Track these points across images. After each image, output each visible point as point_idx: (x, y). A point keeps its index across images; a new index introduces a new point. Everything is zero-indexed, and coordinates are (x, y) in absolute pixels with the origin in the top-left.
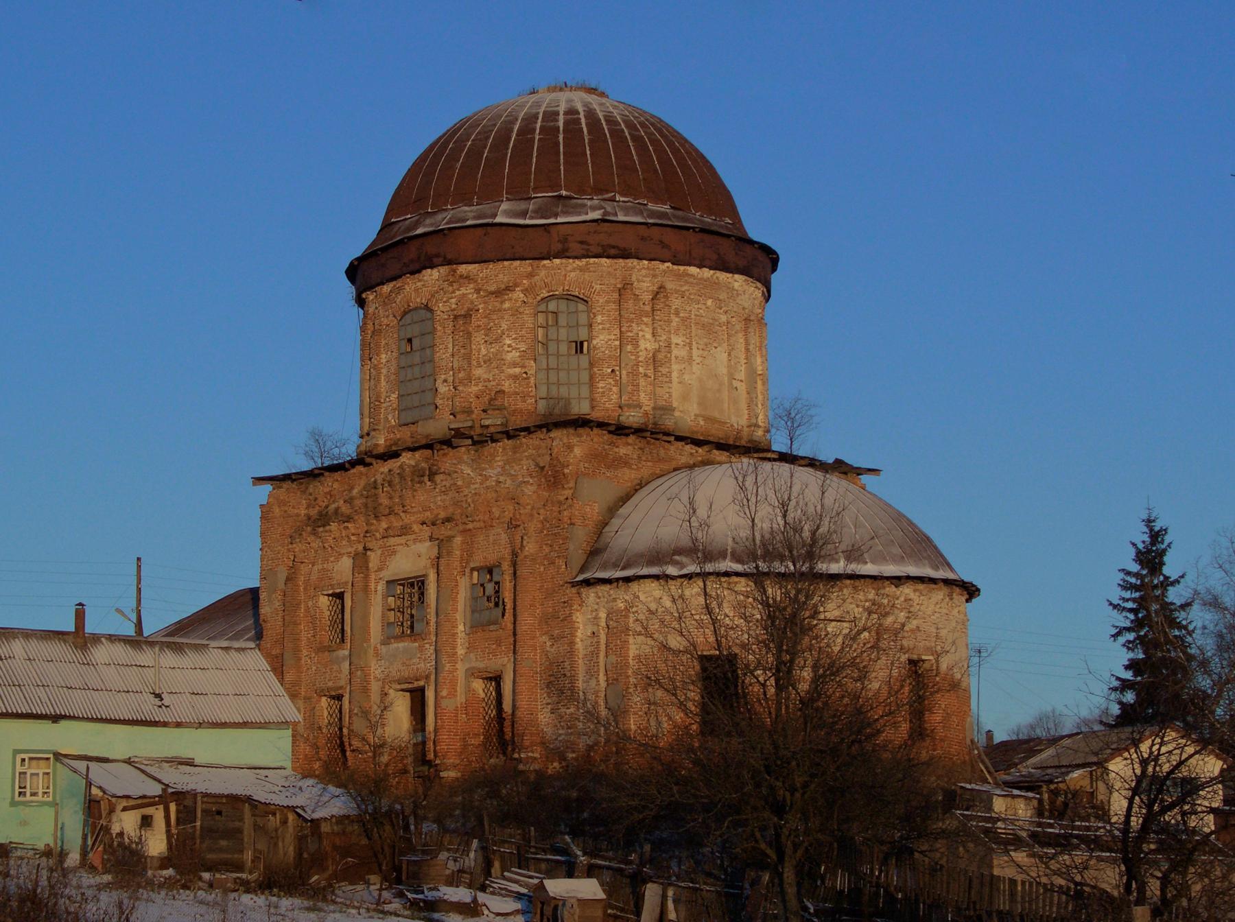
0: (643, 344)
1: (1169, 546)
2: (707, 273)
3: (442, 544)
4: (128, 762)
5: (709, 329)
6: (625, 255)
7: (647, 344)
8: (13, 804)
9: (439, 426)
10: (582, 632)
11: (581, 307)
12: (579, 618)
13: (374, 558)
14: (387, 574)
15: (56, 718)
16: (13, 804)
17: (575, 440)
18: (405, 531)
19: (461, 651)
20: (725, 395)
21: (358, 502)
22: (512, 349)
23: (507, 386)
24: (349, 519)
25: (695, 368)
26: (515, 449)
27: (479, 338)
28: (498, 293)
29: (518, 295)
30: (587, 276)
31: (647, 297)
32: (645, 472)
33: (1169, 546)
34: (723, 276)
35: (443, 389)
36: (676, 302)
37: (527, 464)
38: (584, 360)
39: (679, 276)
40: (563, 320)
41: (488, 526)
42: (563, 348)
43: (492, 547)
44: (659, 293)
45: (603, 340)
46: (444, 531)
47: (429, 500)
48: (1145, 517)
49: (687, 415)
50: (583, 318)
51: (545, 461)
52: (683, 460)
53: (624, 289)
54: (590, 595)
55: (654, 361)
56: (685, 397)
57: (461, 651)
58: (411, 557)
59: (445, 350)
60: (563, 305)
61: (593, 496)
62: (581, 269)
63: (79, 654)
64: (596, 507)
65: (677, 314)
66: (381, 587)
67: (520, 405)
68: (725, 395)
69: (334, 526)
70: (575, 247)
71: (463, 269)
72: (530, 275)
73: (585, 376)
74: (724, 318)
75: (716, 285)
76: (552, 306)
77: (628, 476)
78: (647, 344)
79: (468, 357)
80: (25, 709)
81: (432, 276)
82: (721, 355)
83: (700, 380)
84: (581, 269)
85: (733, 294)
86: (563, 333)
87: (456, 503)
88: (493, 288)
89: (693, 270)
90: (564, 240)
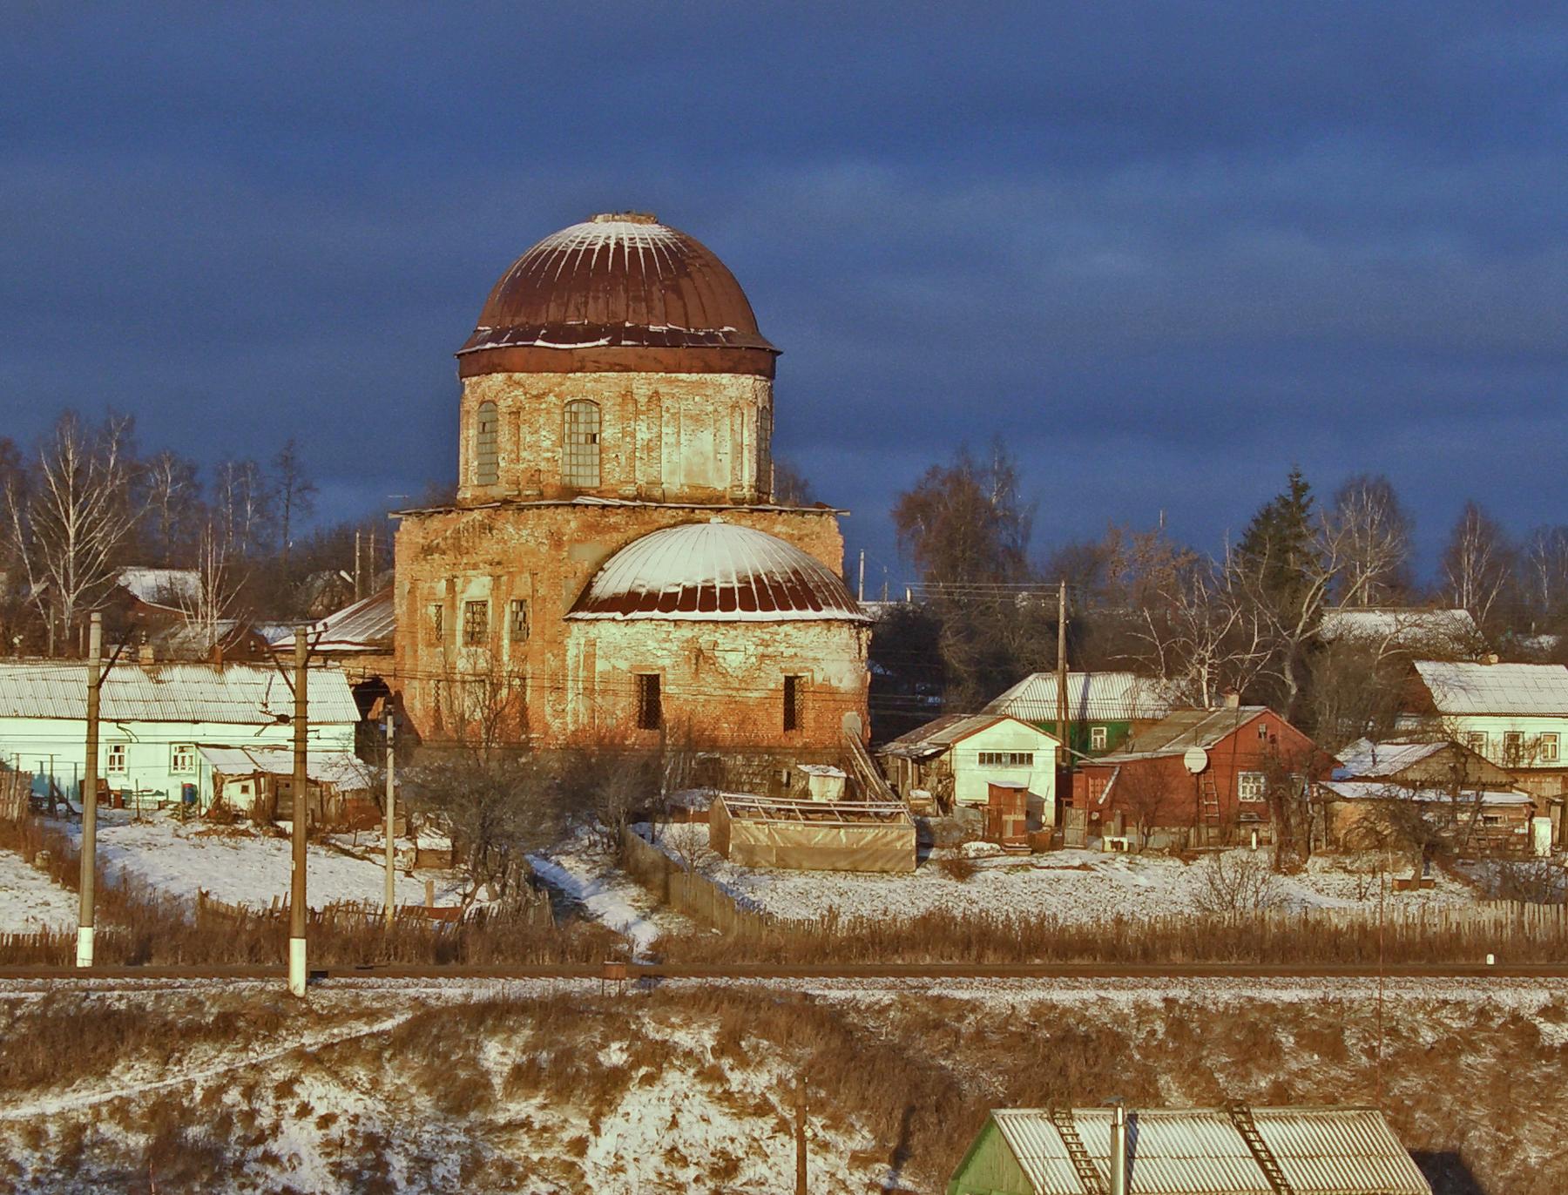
0: (639, 436)
1: (1311, 500)
2: (694, 377)
3: (497, 579)
4: (242, 748)
5: (696, 419)
6: (627, 369)
7: (643, 434)
8: (170, 775)
9: (502, 490)
10: (572, 652)
11: (595, 409)
12: (570, 643)
13: (459, 582)
14: (467, 597)
15: (196, 722)
16: (170, 775)
17: (571, 517)
18: (475, 567)
19: (505, 658)
20: (710, 466)
21: (450, 541)
22: (547, 439)
23: (543, 466)
24: (444, 553)
25: (683, 449)
26: (540, 516)
27: (525, 429)
28: (538, 397)
29: (552, 398)
30: (599, 386)
31: (643, 400)
32: (631, 533)
33: (1311, 500)
34: (708, 376)
35: (502, 464)
36: (667, 402)
37: (545, 529)
38: (596, 448)
39: (670, 382)
40: (582, 418)
41: (521, 572)
42: (582, 439)
43: (523, 587)
44: (656, 396)
45: (609, 433)
46: (499, 570)
47: (489, 547)
48: (1291, 471)
49: (674, 483)
50: (596, 417)
51: (554, 528)
52: (664, 522)
53: (627, 395)
54: (574, 627)
55: (649, 448)
56: (672, 473)
57: (505, 658)
58: (478, 587)
59: (504, 436)
60: (582, 407)
61: (585, 556)
62: (595, 381)
63: (217, 677)
64: (586, 564)
65: (668, 410)
66: (463, 605)
67: (551, 480)
68: (710, 466)
69: (436, 556)
70: (590, 365)
71: (517, 376)
72: (561, 384)
73: (596, 460)
74: (711, 408)
75: (704, 384)
76: (574, 408)
77: (618, 537)
78: (643, 434)
79: (517, 444)
80: (175, 717)
81: (499, 377)
82: (707, 436)
83: (687, 458)
84: (595, 381)
85: (720, 388)
86: (582, 428)
87: (505, 552)
88: (535, 393)
89: (683, 376)
90: (582, 360)
